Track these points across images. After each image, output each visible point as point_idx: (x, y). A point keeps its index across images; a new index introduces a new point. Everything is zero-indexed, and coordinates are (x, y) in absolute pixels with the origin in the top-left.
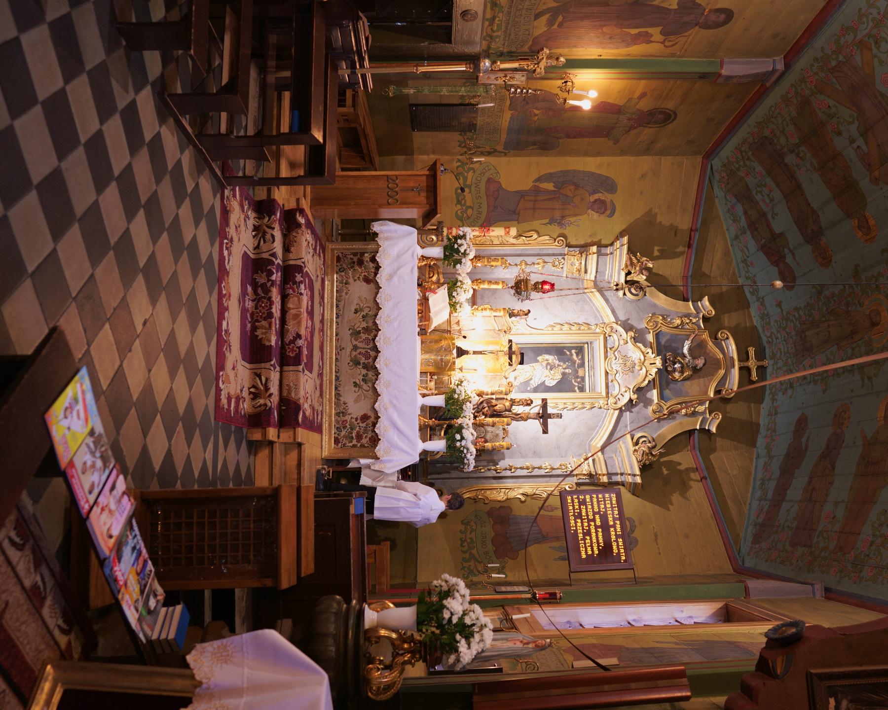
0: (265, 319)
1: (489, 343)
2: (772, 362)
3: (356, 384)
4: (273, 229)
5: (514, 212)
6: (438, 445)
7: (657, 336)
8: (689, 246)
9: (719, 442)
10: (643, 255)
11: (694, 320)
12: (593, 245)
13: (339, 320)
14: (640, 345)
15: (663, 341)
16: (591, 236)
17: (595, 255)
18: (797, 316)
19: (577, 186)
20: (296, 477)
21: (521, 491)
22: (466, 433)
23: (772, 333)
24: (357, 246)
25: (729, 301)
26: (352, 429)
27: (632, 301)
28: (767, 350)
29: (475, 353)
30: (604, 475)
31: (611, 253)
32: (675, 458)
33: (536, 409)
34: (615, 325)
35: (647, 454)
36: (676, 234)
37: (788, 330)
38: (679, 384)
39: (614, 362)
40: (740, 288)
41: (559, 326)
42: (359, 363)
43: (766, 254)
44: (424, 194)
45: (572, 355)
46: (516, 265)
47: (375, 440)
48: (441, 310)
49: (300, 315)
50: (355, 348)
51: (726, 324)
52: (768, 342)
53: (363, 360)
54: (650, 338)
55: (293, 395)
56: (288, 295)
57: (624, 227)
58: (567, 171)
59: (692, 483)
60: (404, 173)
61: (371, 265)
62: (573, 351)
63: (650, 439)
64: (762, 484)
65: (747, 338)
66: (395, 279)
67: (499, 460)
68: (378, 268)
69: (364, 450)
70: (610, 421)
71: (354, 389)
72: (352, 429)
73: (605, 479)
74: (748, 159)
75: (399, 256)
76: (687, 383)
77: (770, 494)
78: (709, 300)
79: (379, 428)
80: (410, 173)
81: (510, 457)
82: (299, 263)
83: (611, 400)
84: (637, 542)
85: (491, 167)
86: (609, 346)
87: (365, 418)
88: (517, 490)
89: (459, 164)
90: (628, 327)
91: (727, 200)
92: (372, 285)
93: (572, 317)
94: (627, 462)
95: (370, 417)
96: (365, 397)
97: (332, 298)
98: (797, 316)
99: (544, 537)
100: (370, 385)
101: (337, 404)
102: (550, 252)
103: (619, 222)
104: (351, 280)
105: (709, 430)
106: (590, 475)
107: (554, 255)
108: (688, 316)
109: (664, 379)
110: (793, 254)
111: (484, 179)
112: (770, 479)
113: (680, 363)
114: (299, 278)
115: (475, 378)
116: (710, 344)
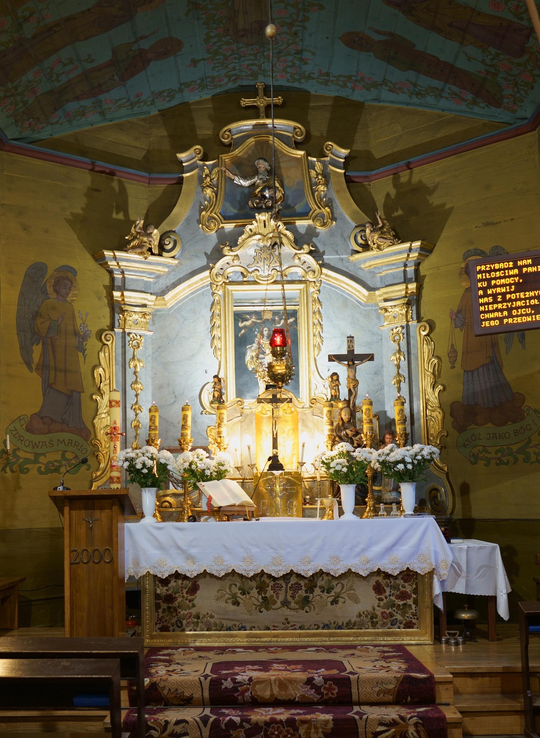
0: (297, 730)
1: (259, 430)
2: (261, 78)
3: (335, 602)
4: (167, 722)
5: (70, 397)
6: (408, 493)
7: (227, 218)
8: (112, 173)
9: (358, 146)
10: (128, 233)
11: (207, 171)
12: (112, 296)
13: (248, 626)
14: (240, 240)
15: (234, 211)
16: (99, 299)
17: (126, 293)
18: (215, 40)
19: (37, 314)
20: (487, 679)
21: (429, 390)
22: (392, 458)
23: (226, 76)
24: (147, 602)
25: (180, 128)
26: (393, 605)
27: (183, 250)
28: (245, 83)
29: (275, 446)
30: (407, 288)
31: (123, 273)
32: (379, 200)
33: (342, 369)
34: (214, 271)
35: (383, 233)
36: (97, 190)
37: (228, 54)
38: (287, 192)
39: (261, 273)
40: (163, 113)
41: (215, 341)
42: (306, 598)
43: (132, 75)
44: (97, 514)
45: (245, 327)
46: (137, 395)
47: (408, 575)
48: (230, 490)
49: (279, 680)
50: (286, 603)
51: (209, 132)
52: (235, 81)
53: (302, 593)
54: (229, 227)
55: (391, 687)
56: (252, 697)
57: (88, 256)
58: (18, 326)
59: (415, 179)
60: (67, 541)
61: (173, 584)
62: (241, 325)
63: (358, 230)
64: (418, 94)
65: (230, 106)
66: (193, 551)
67: (387, 417)
68: (177, 575)
69: (420, 588)
70: (336, 279)
71: (340, 603)
72: (393, 605)
73: (412, 287)
74: (16, 88)
75: (161, 547)
76: (286, 182)
77: (437, 84)
78: (182, 152)
79: (277, 572)
80: (66, 533)
81: (383, 404)
82: (206, 684)
83: (310, 277)
84: (497, 247)
85: (12, 427)
86: (241, 279)
87: (378, 589)
88: (428, 395)
89: (8, 469)
90: (216, 255)
91: (57, 123)
92: (200, 582)
93: (203, 325)
94: (392, 257)
95: (377, 582)
96: (351, 589)
97: (219, 636)
98: (215, 40)
99: (493, 361)
100: (335, 583)
101: (361, 625)
102: (120, 351)
103: (83, 263)
104: (194, 611)
105: (345, 158)
106: (408, 304)
107: (124, 347)
108: (201, 180)
109: (286, 213)
110: (142, 38)
111: (28, 436)
112: (415, 85)
113: (263, 190)
114: (228, 684)
115: (309, 446)
116: (237, 152)
